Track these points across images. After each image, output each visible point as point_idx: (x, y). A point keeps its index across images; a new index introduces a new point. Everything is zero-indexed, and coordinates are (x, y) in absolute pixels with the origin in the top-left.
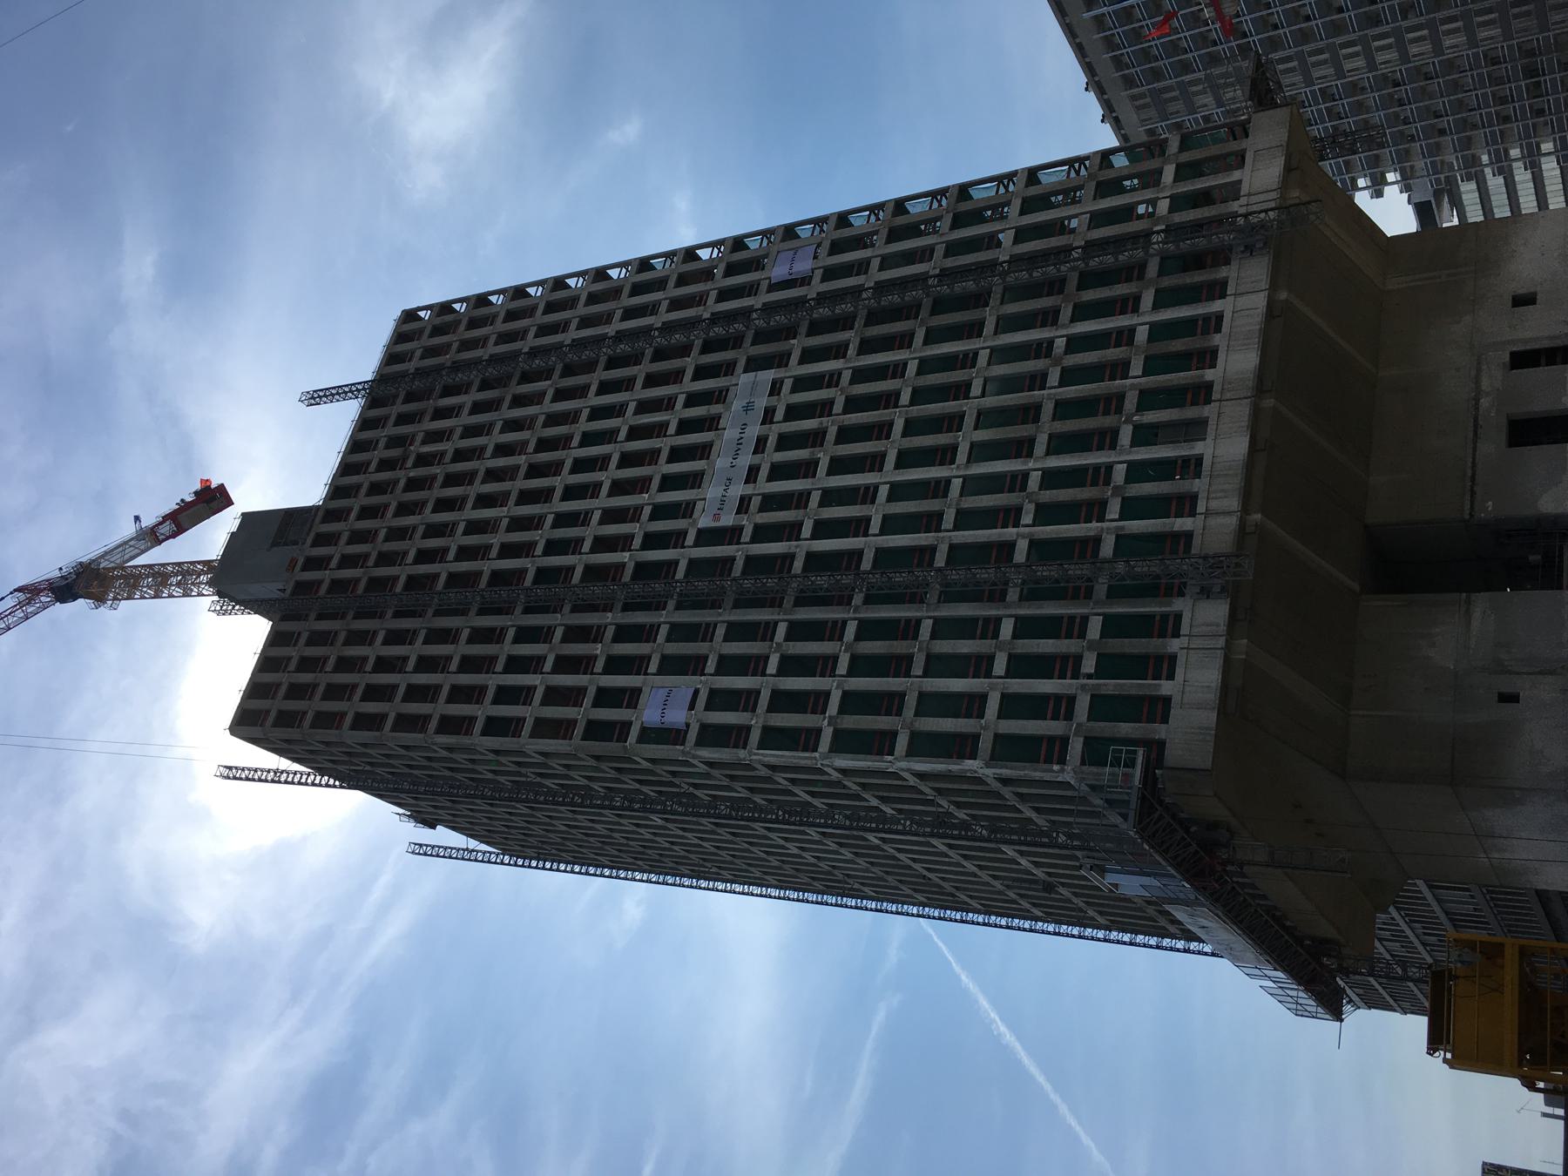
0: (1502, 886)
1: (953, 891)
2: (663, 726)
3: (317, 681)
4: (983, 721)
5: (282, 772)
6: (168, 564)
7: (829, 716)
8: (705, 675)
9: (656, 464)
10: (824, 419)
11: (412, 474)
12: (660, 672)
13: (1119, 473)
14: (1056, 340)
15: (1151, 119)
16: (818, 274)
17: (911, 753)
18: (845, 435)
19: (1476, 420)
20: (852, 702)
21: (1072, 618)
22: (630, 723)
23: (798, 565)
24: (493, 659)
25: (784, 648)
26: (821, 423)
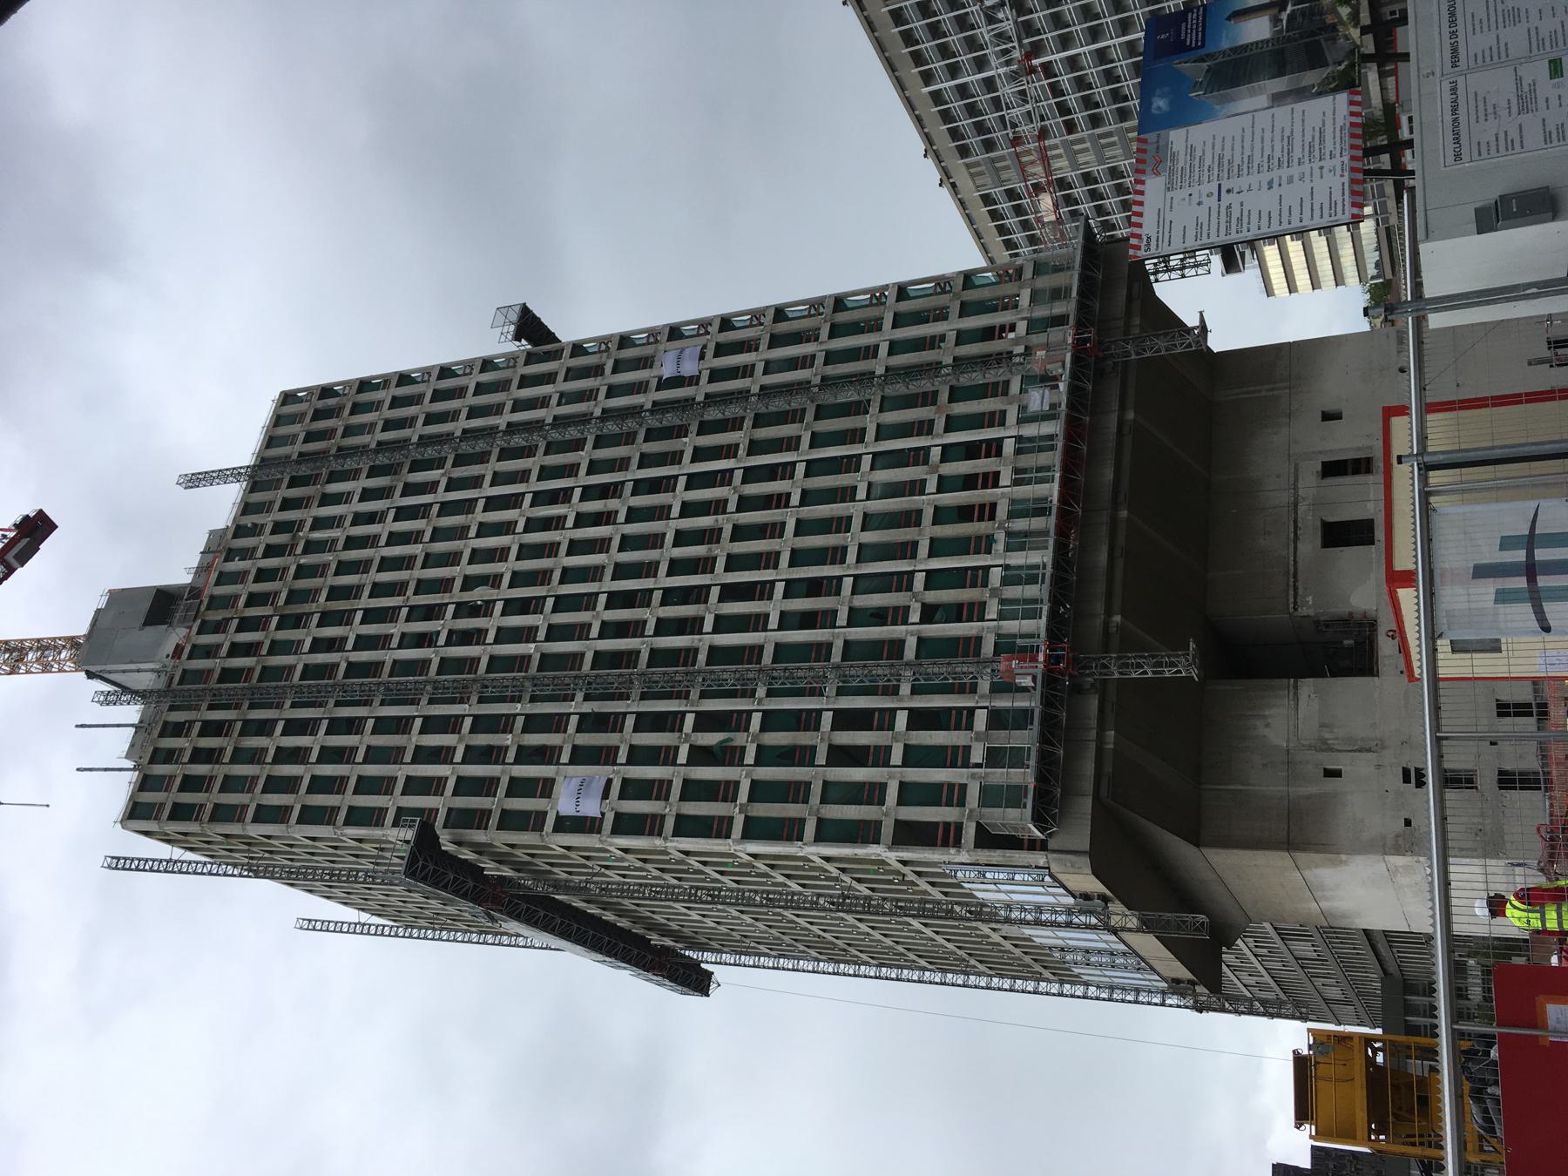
0: (1331, 928)
1: (846, 947)
2: (578, 814)
3: (214, 774)
4: (884, 808)
5: (176, 862)
6: (26, 640)
7: (741, 804)
8: (617, 765)
9: (556, 556)
10: (720, 517)
11: (302, 561)
12: (572, 762)
13: (996, 576)
14: (933, 448)
15: (985, 185)
16: (705, 375)
17: (819, 838)
18: (739, 533)
19: (1295, 522)
20: (760, 791)
21: (959, 710)
22: (545, 813)
23: (702, 657)
24: (401, 750)
25: (693, 738)
26: (717, 521)
